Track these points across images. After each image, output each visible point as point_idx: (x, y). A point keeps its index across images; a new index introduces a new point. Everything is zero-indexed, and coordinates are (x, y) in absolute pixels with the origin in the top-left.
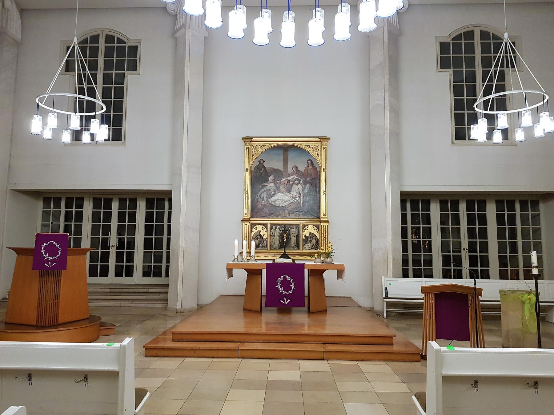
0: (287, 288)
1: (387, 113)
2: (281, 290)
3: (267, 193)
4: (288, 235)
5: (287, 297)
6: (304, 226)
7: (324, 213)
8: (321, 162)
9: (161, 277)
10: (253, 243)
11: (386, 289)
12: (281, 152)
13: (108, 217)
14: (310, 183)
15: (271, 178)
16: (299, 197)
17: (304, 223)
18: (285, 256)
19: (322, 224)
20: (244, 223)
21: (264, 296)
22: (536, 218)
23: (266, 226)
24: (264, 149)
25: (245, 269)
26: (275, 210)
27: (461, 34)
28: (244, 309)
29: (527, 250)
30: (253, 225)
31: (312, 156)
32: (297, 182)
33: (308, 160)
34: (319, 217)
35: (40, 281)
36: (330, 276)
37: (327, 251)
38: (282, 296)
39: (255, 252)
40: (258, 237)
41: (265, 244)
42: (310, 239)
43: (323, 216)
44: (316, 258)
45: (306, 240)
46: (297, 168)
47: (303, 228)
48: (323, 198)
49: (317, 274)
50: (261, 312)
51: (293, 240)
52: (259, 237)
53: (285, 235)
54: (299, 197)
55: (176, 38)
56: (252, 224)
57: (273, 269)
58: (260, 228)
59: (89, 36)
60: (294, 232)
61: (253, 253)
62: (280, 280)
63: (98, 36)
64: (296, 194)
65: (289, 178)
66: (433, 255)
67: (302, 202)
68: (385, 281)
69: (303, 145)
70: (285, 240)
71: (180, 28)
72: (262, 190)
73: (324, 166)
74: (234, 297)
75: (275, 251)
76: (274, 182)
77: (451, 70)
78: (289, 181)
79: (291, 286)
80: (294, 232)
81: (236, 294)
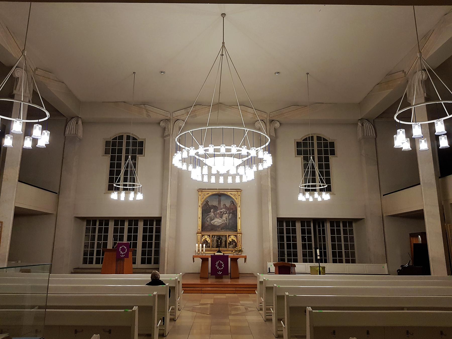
0: (220, 267)
1: (269, 179)
2: (218, 267)
3: (210, 218)
4: (221, 241)
5: (221, 271)
6: (229, 236)
7: (239, 229)
8: (238, 201)
9: (151, 264)
10: (204, 245)
11: (269, 268)
12: (217, 197)
13: (122, 230)
14: (232, 213)
15: (212, 210)
16: (227, 220)
17: (229, 234)
18: (219, 251)
19: (238, 235)
20: (198, 234)
21: (210, 273)
22: (351, 232)
23: (209, 236)
24: (208, 195)
25: (201, 258)
26: (214, 228)
27: (307, 138)
28: (200, 278)
29: (316, 249)
30: (203, 236)
31: (233, 199)
32: (225, 212)
33: (231, 201)
34: (237, 231)
35: (116, 263)
36: (240, 261)
37: (239, 249)
38: (218, 271)
39: (205, 250)
40: (206, 242)
41: (209, 245)
42: (232, 243)
43: (239, 231)
44: (234, 253)
45: (230, 243)
46: (225, 205)
47: (229, 237)
48: (239, 221)
49: (235, 260)
50: (208, 278)
51: (223, 243)
52: (206, 242)
53: (219, 241)
54: (227, 220)
55: (165, 140)
56: (202, 235)
57: (214, 258)
58: (206, 237)
59: (117, 136)
60: (224, 239)
61: (204, 250)
62: (217, 263)
63: (123, 136)
64: (225, 219)
65: (221, 211)
66: (298, 251)
67: (228, 223)
68: (269, 264)
69: (229, 193)
70: (219, 244)
71: (167, 136)
72: (208, 217)
73: (239, 204)
74: (193, 274)
75: (214, 249)
76: (214, 212)
77: (302, 156)
78: (221, 212)
79: (222, 265)
80: (224, 239)
81: (195, 272)
